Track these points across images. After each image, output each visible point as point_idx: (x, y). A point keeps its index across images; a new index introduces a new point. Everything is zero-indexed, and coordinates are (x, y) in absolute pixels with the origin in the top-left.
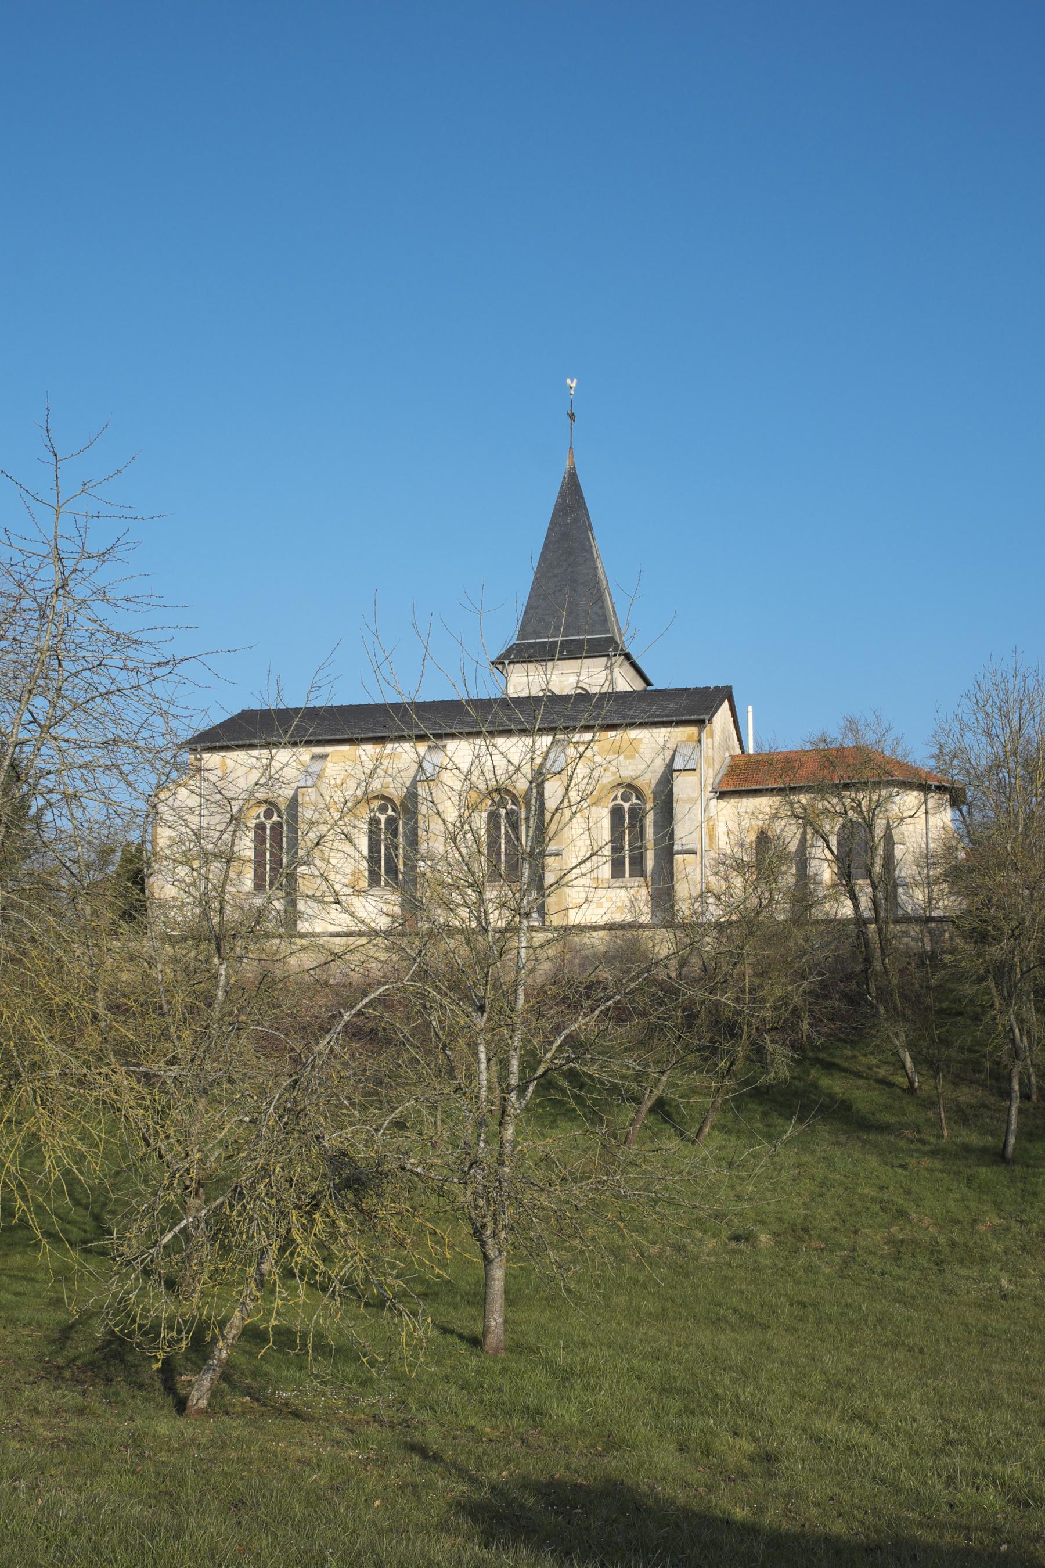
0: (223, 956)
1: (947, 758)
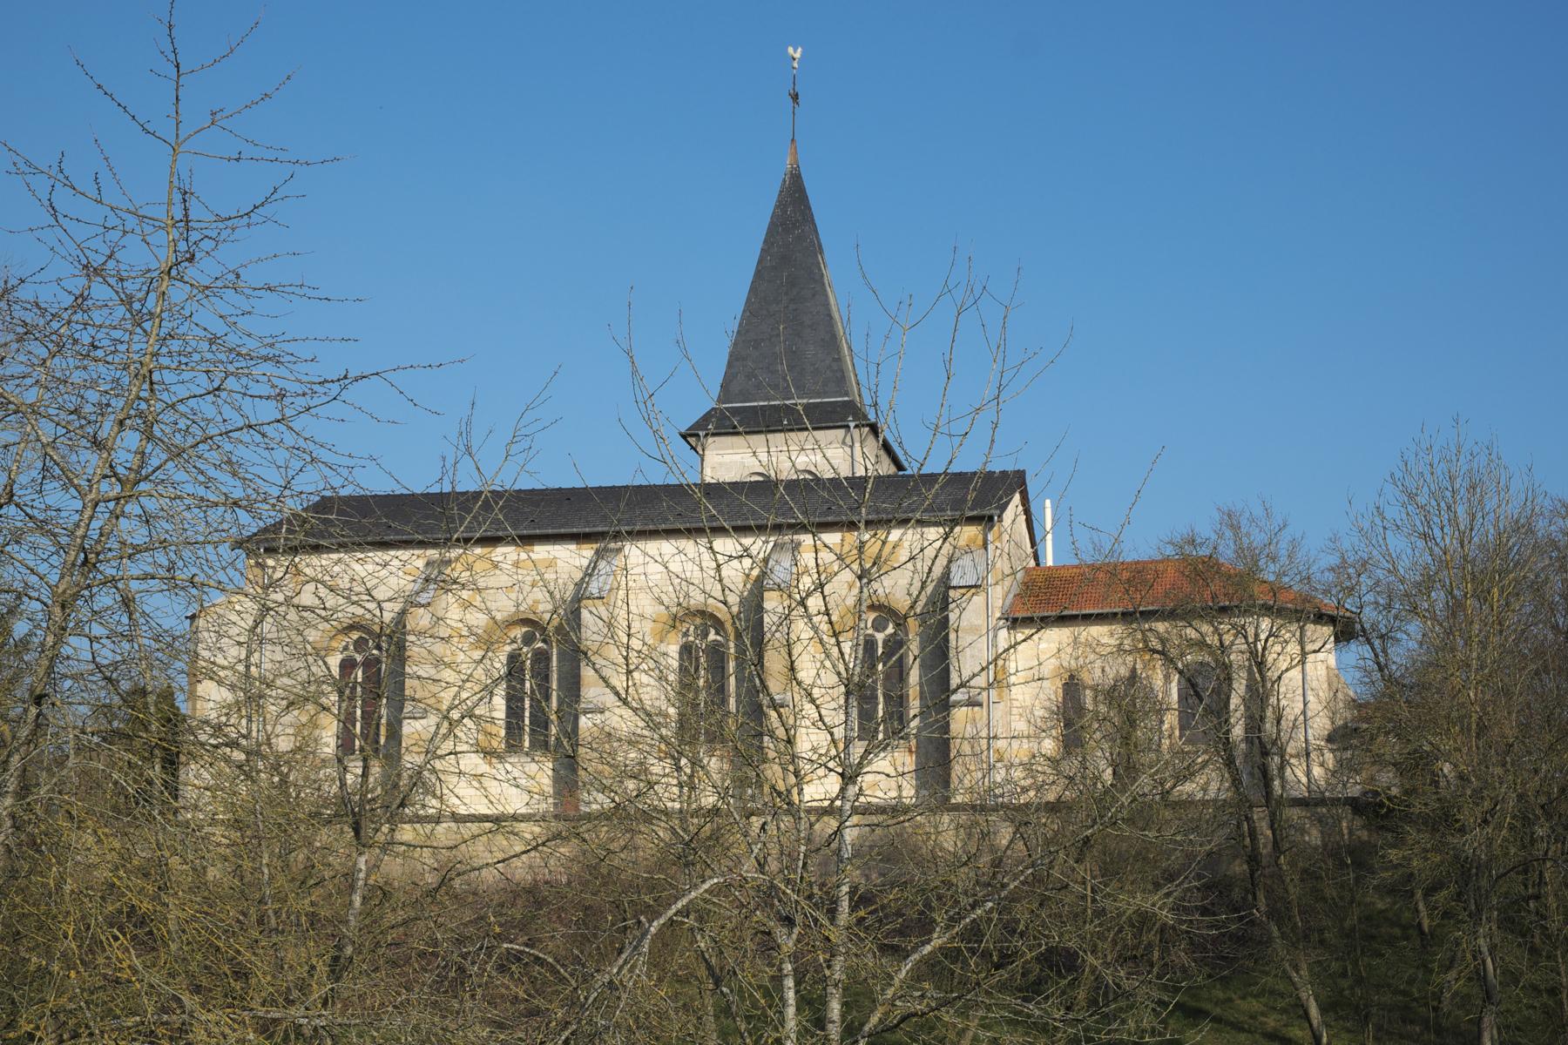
0: (363, 841)
1: (1351, 570)
